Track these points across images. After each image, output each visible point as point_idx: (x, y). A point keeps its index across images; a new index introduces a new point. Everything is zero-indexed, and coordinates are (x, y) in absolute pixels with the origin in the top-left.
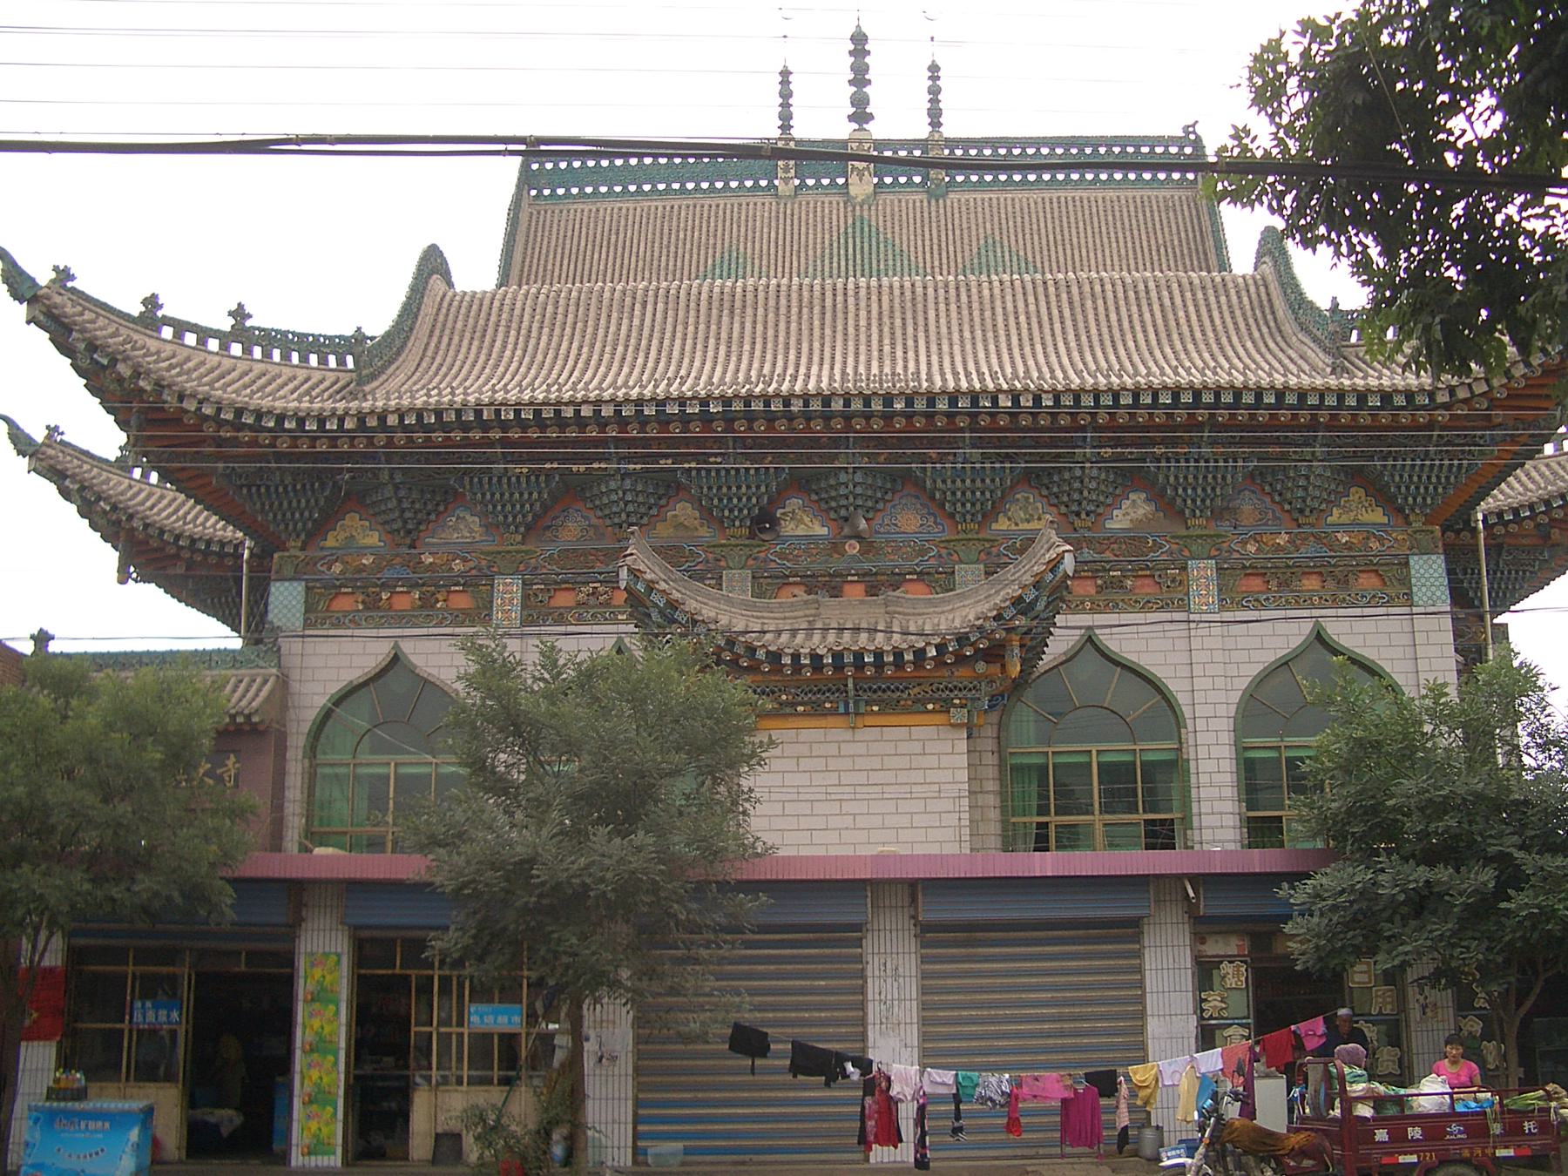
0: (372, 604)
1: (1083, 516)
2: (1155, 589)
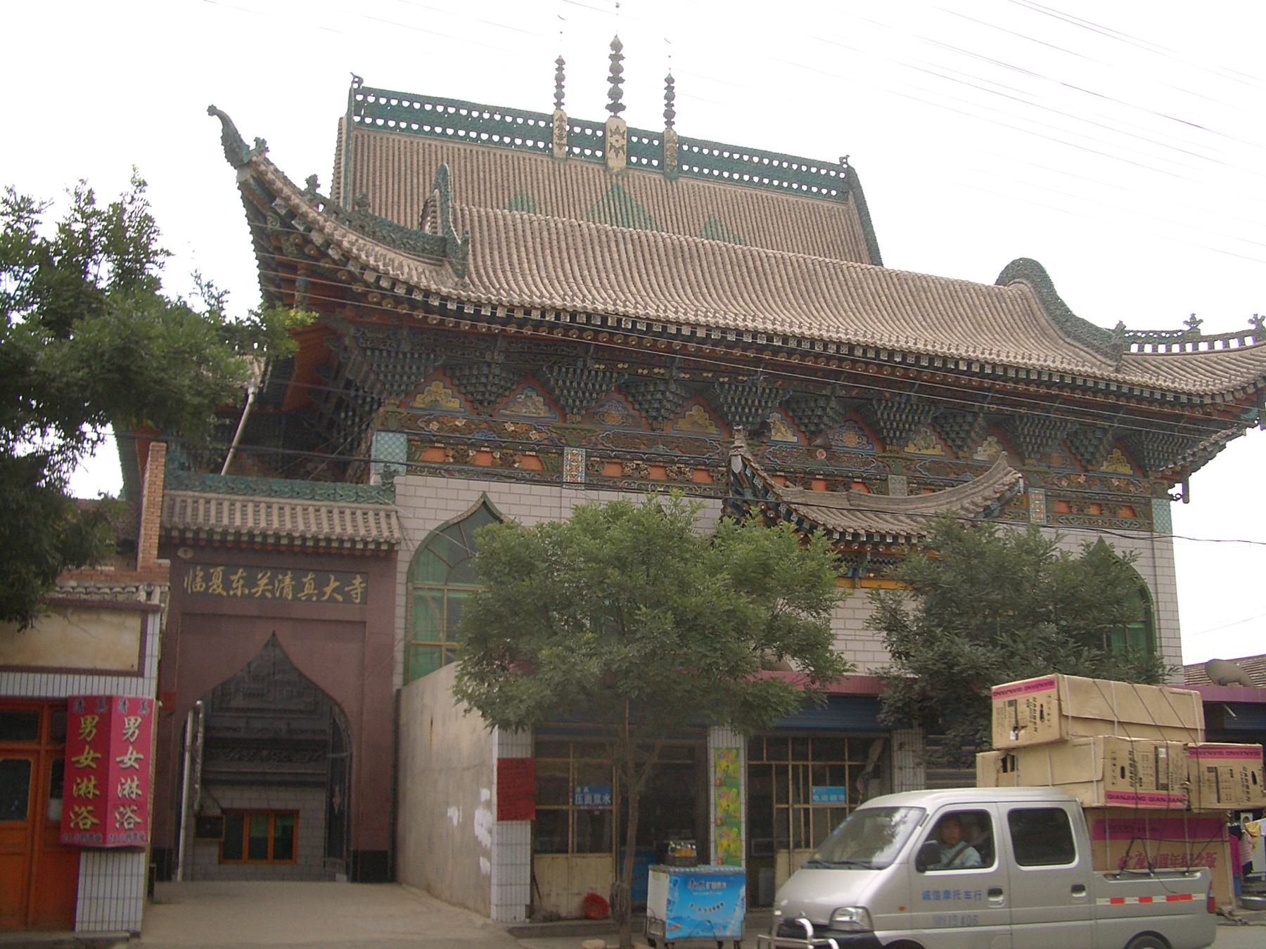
0: (461, 459)
2: (708, 480)
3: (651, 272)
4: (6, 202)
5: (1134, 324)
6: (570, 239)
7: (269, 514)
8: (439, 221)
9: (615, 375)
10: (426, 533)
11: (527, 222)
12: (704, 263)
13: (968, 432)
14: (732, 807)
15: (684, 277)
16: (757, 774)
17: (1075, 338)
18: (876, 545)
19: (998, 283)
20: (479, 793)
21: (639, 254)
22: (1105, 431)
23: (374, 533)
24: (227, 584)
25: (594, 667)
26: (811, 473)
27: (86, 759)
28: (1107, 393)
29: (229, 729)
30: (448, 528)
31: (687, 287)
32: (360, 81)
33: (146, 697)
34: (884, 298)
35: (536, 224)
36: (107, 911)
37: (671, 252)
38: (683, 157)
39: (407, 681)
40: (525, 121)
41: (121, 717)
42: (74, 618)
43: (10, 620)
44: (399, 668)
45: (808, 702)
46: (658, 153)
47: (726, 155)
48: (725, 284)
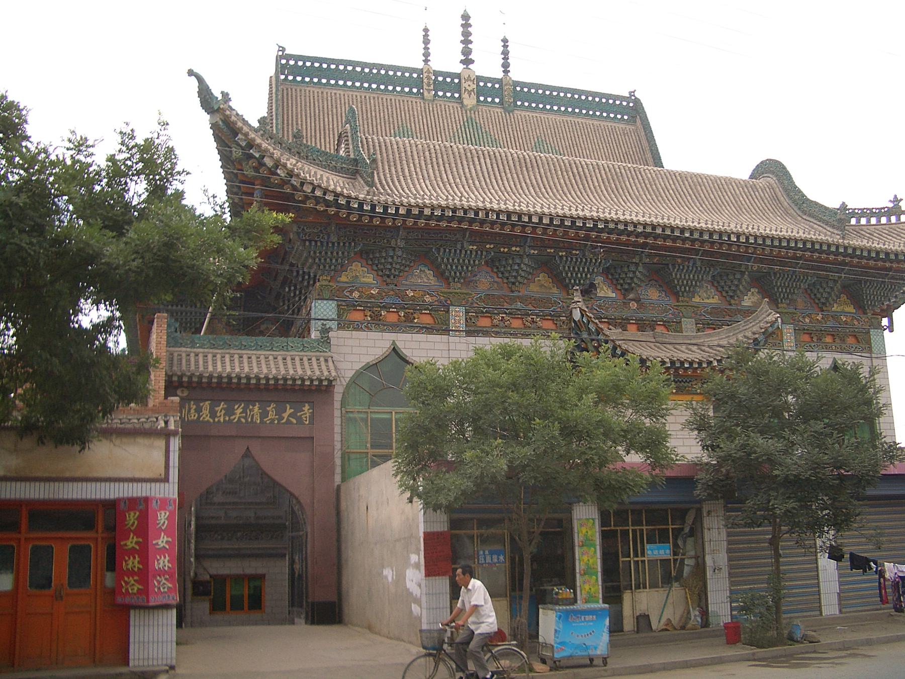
1: (392, 277)
2: (554, 327)
3: (505, 178)
4: (70, 141)
5: (853, 204)
6: (445, 156)
7: (241, 362)
8: (351, 147)
9: (484, 253)
10: (354, 372)
11: (414, 145)
12: (542, 170)
13: (737, 286)
14: (591, 561)
15: (528, 181)
16: (606, 536)
17: (810, 215)
18: (677, 369)
19: (751, 177)
20: (409, 558)
21: (495, 165)
22: (835, 281)
23: (318, 373)
24: (213, 414)
25: (503, 464)
26: (627, 319)
27: (131, 542)
28: (837, 253)
29: (212, 518)
30: (369, 367)
31: (531, 188)
32: (284, 50)
33: (171, 496)
34: (671, 191)
35: (420, 146)
36: (151, 652)
37: (517, 164)
38: (517, 96)
39: (344, 480)
40: (403, 74)
41: (156, 511)
42: (118, 442)
43: (73, 444)
44: (338, 470)
45: (652, 485)
46: (500, 93)
47: (548, 93)
48: (558, 185)
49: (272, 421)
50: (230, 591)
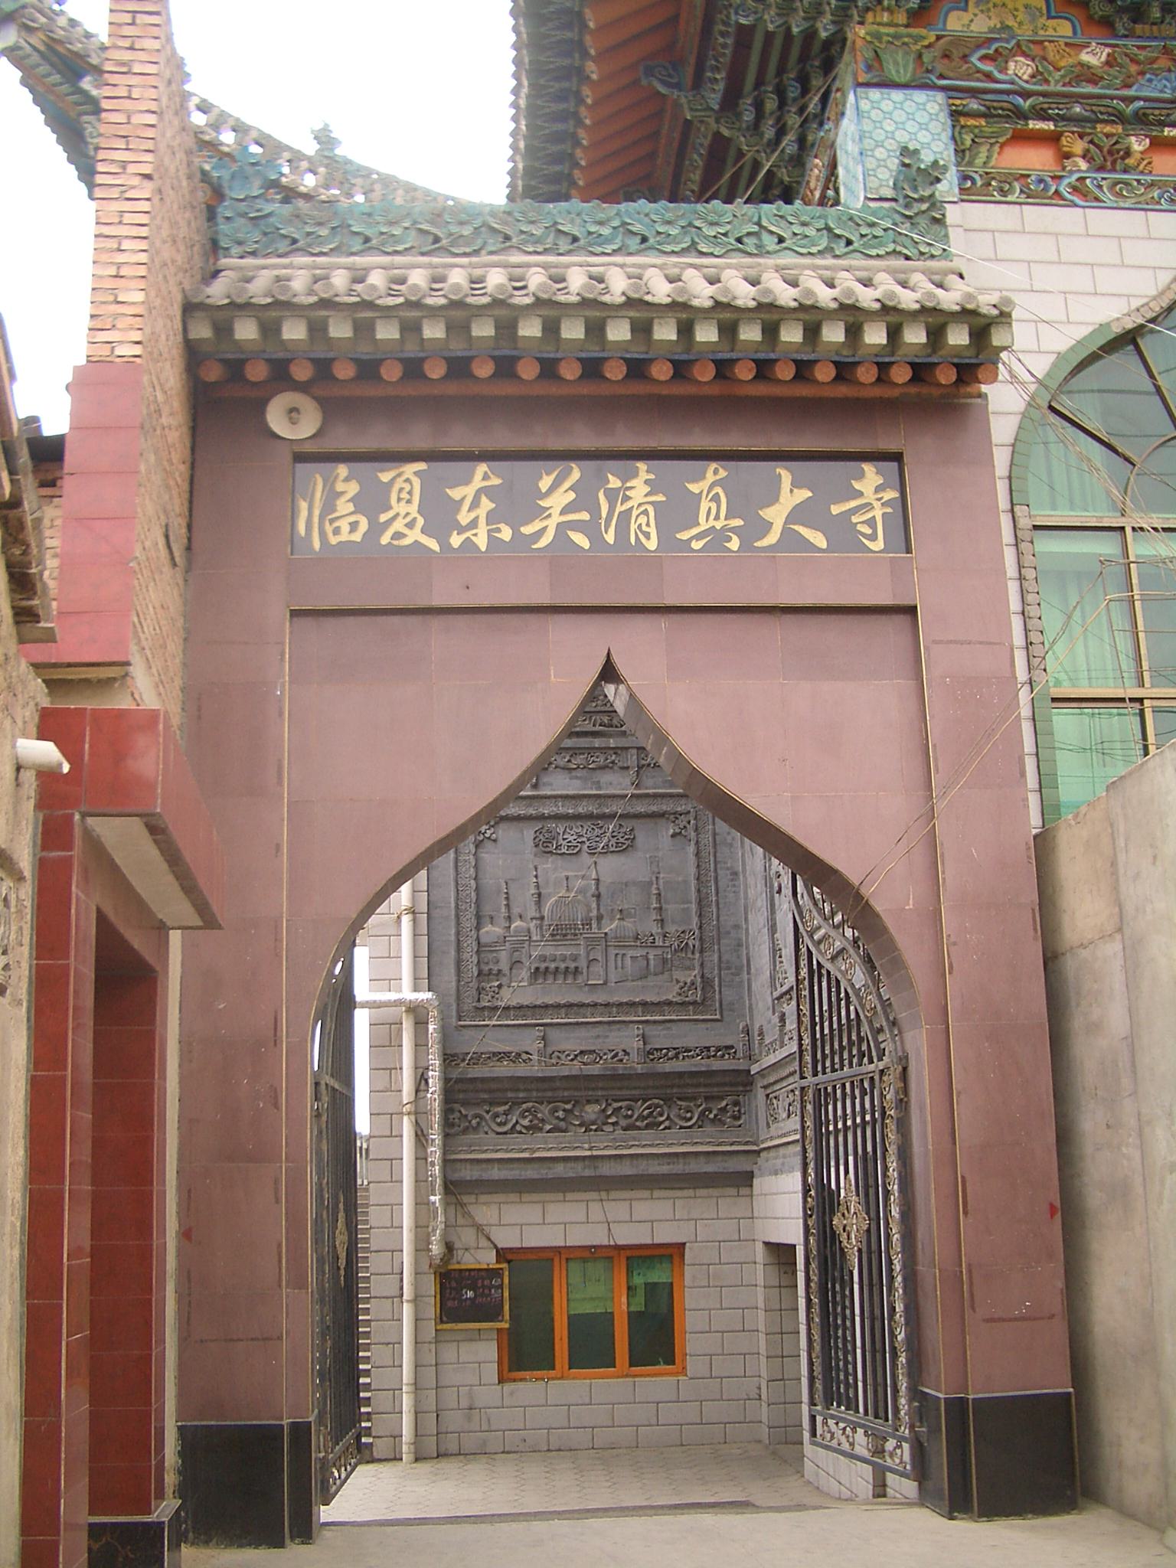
49: (718, 538)
50: (572, 1298)
